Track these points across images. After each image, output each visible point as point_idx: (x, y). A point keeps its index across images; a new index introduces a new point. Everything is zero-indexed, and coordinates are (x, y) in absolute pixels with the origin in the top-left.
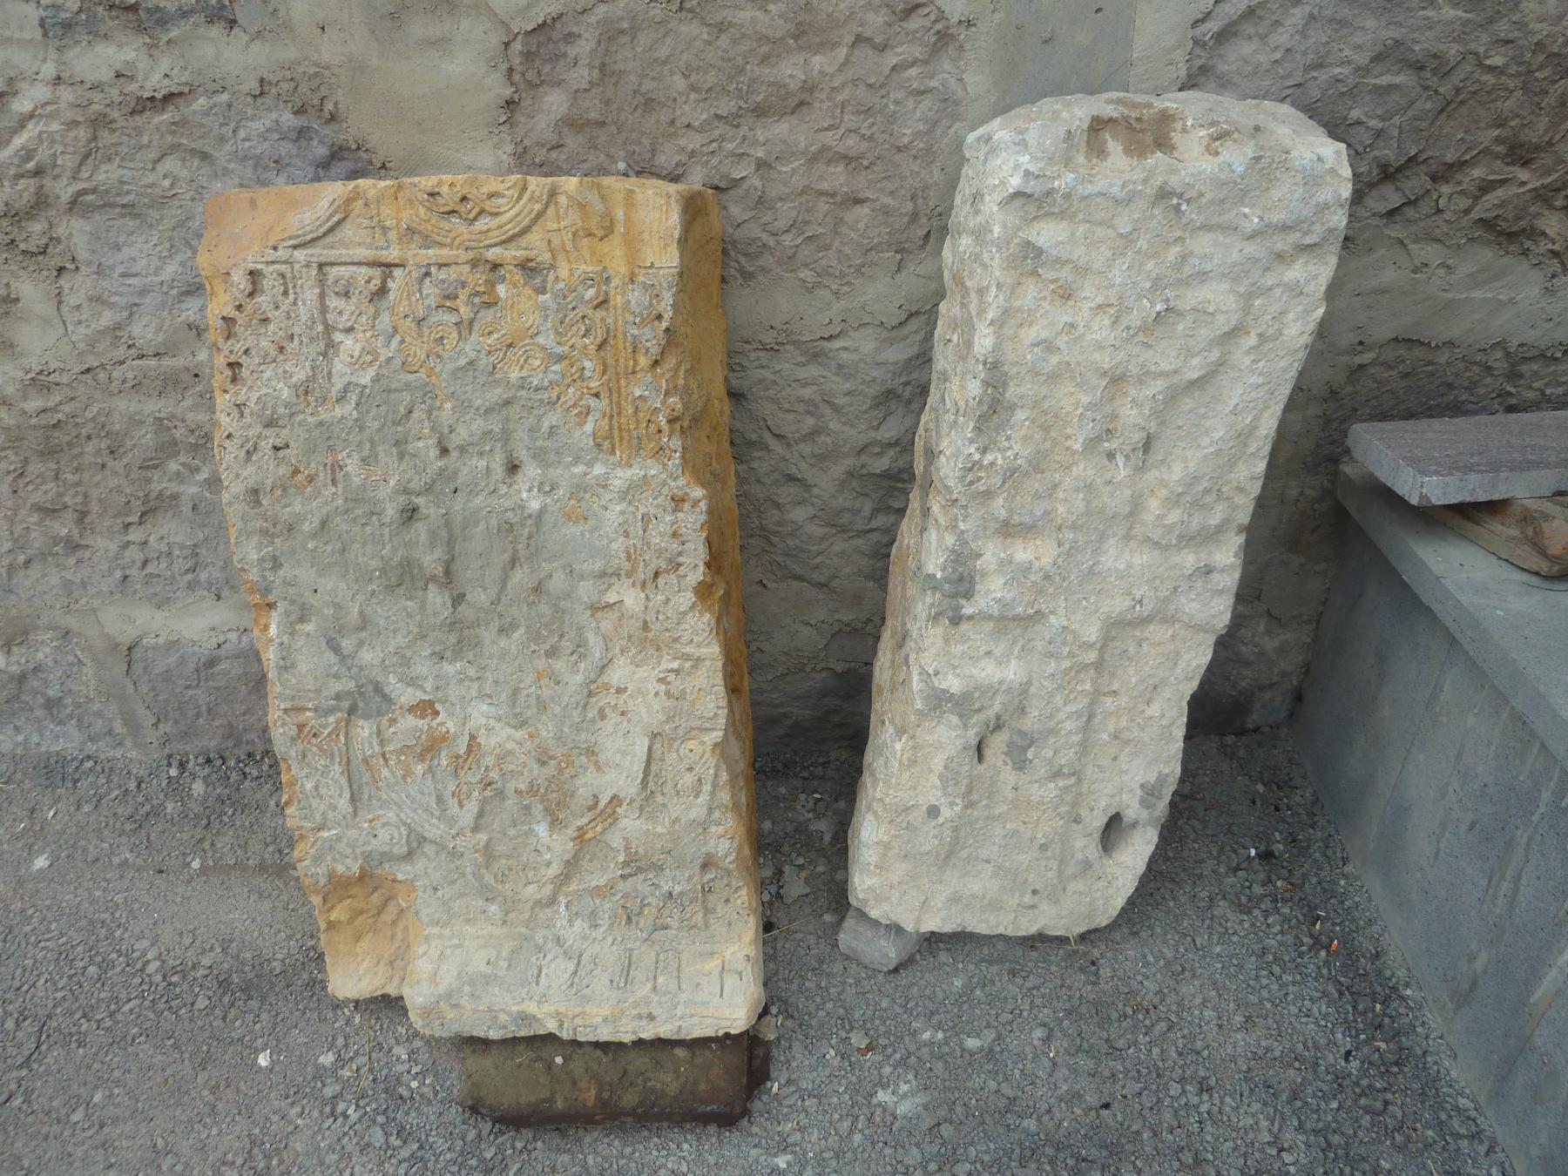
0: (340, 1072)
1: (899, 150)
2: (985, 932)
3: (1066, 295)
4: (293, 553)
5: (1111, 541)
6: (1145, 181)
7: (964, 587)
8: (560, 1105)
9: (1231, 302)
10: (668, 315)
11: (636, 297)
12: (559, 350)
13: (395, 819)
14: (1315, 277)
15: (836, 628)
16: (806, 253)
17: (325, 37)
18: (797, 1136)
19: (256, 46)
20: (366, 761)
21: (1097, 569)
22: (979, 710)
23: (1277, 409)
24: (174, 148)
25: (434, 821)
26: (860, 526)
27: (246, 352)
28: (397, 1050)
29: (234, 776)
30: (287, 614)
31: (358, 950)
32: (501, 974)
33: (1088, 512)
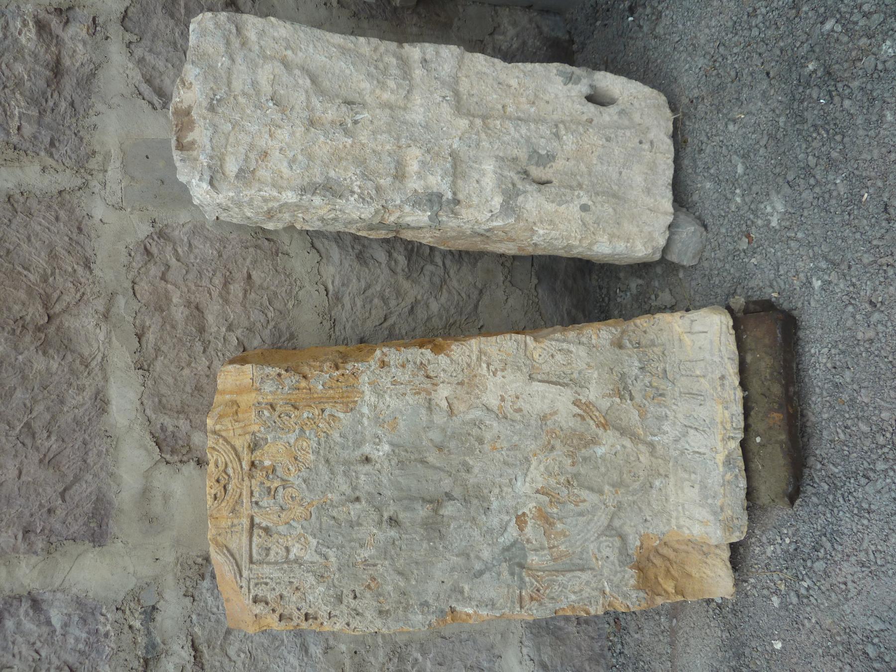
0: (783, 592)
1: (220, 256)
2: (672, 171)
3: (265, 154)
4: (418, 594)
5: (407, 117)
6: (205, 119)
7: (435, 198)
8: (783, 437)
9: (268, 67)
10: (278, 370)
11: (268, 387)
12: (297, 431)
13: (595, 543)
14: (254, 24)
15: (508, 284)
16: (278, 305)
17: (161, 558)
18: (802, 275)
19: (167, 596)
20: (555, 560)
21: (423, 124)
22: (514, 185)
23: (328, 35)
24: (222, 648)
25: (595, 518)
26: (441, 272)
27: (299, 609)
28: (769, 554)
29: (622, 660)
30: (457, 600)
31: (697, 575)
32: (699, 478)
33: (389, 133)
